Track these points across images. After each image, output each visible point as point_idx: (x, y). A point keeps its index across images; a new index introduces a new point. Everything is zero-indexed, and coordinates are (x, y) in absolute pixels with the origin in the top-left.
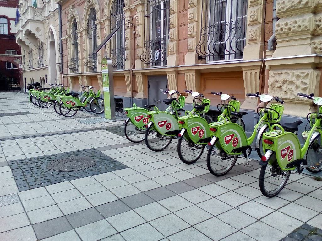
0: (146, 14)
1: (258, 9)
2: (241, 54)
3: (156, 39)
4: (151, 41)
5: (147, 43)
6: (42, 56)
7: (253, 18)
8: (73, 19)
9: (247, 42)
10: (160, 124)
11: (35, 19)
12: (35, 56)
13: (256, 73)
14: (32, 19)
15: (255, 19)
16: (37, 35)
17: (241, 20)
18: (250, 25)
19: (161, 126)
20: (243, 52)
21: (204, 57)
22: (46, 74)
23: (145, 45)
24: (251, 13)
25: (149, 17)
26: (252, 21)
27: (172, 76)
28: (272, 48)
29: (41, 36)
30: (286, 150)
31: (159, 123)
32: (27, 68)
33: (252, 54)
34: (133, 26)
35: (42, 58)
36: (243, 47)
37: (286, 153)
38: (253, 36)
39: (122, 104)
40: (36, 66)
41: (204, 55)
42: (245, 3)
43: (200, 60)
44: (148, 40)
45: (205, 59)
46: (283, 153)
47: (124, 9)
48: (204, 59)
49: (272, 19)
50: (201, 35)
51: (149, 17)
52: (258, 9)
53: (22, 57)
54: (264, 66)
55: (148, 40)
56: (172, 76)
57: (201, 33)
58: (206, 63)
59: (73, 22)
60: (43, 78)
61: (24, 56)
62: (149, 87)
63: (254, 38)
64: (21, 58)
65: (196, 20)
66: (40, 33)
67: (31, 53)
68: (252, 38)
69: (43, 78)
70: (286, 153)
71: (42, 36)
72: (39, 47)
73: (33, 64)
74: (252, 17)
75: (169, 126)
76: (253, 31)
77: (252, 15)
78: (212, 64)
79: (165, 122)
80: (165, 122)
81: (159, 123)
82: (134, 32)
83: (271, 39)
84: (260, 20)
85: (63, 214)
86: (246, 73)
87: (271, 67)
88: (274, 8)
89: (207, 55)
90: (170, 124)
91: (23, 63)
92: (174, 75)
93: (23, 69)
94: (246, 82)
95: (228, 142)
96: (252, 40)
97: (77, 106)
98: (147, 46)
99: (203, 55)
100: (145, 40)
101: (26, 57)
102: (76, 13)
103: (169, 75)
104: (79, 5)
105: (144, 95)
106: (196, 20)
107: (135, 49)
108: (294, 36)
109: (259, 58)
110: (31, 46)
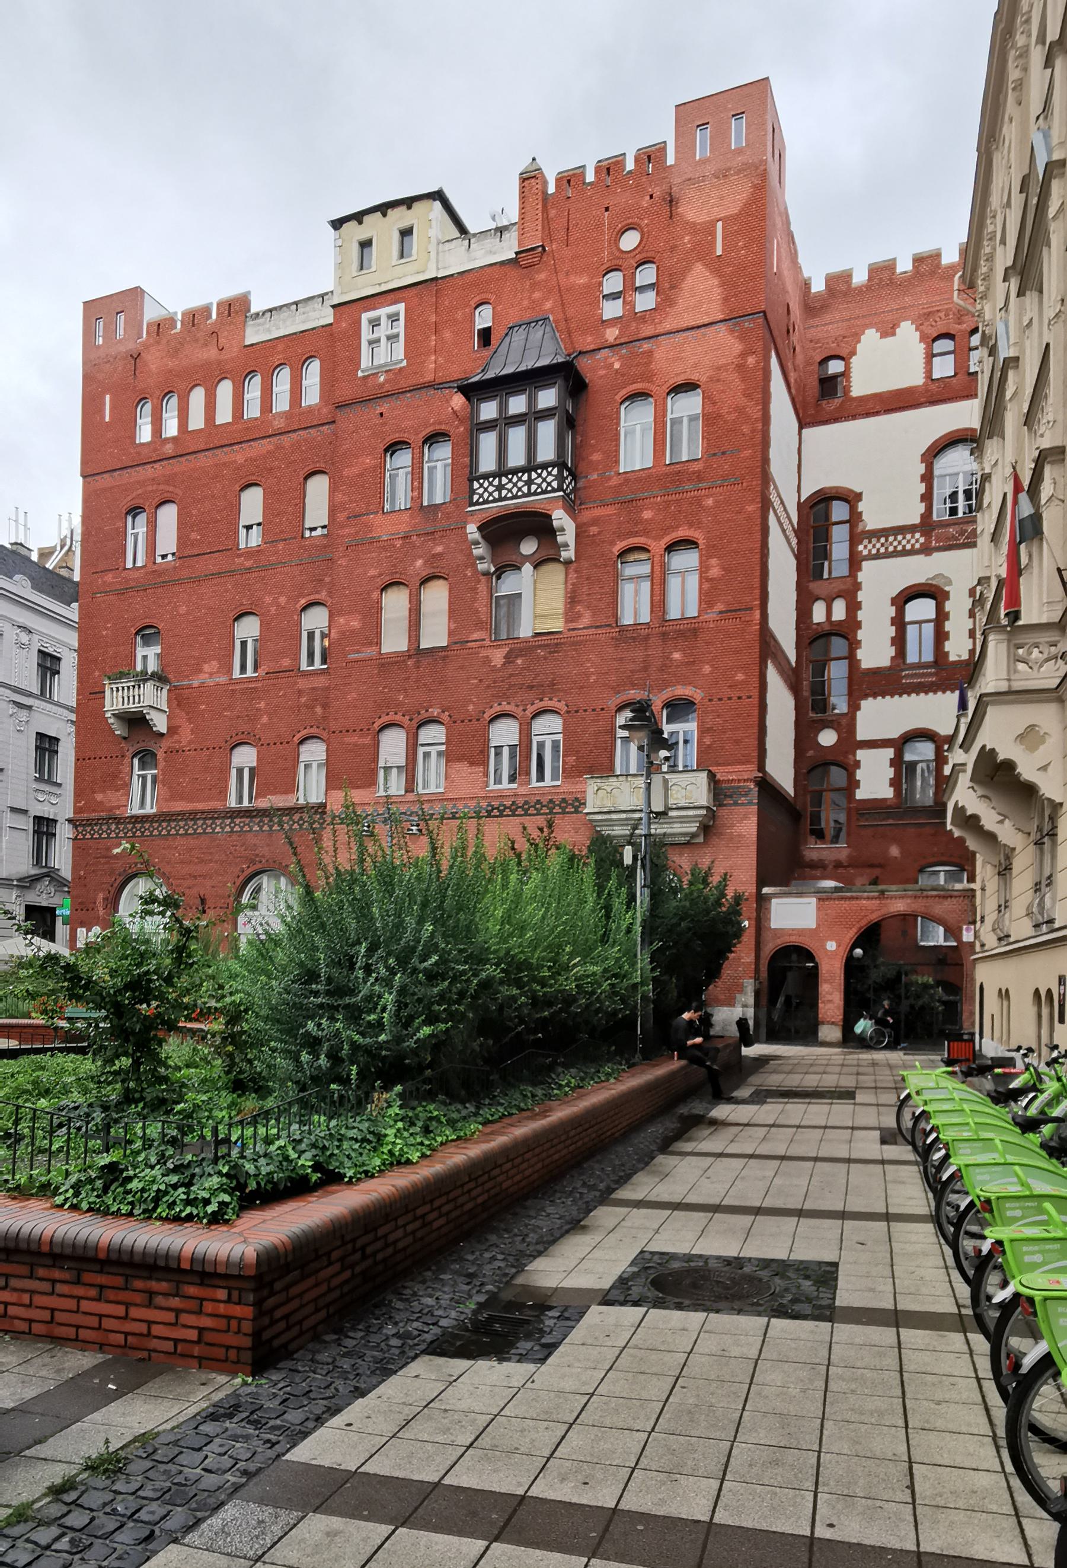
1: (1002, 1141)
6: (1050, 877)
11: (1017, 686)
12: (1022, 882)
14: (1003, 687)
16: (1027, 771)
22: (1062, 973)
29: (1044, 768)
32: (990, 940)
35: (1000, 906)
40: (1021, 929)
42: (657, 598)
48: (150, 1303)
52: (1002, 1141)
53: (978, 893)
60: (1049, 992)
61: (983, 889)
64: (974, 896)
66: (1042, 754)
67: (1004, 871)
69: (1049, 992)
71: (1050, 769)
72: (1040, 829)
73: (1054, 900)
85: (918, 1545)
91: (978, 918)
93: (978, 948)
101: (988, 892)
105: (1045, 1383)
110: (1007, 833)
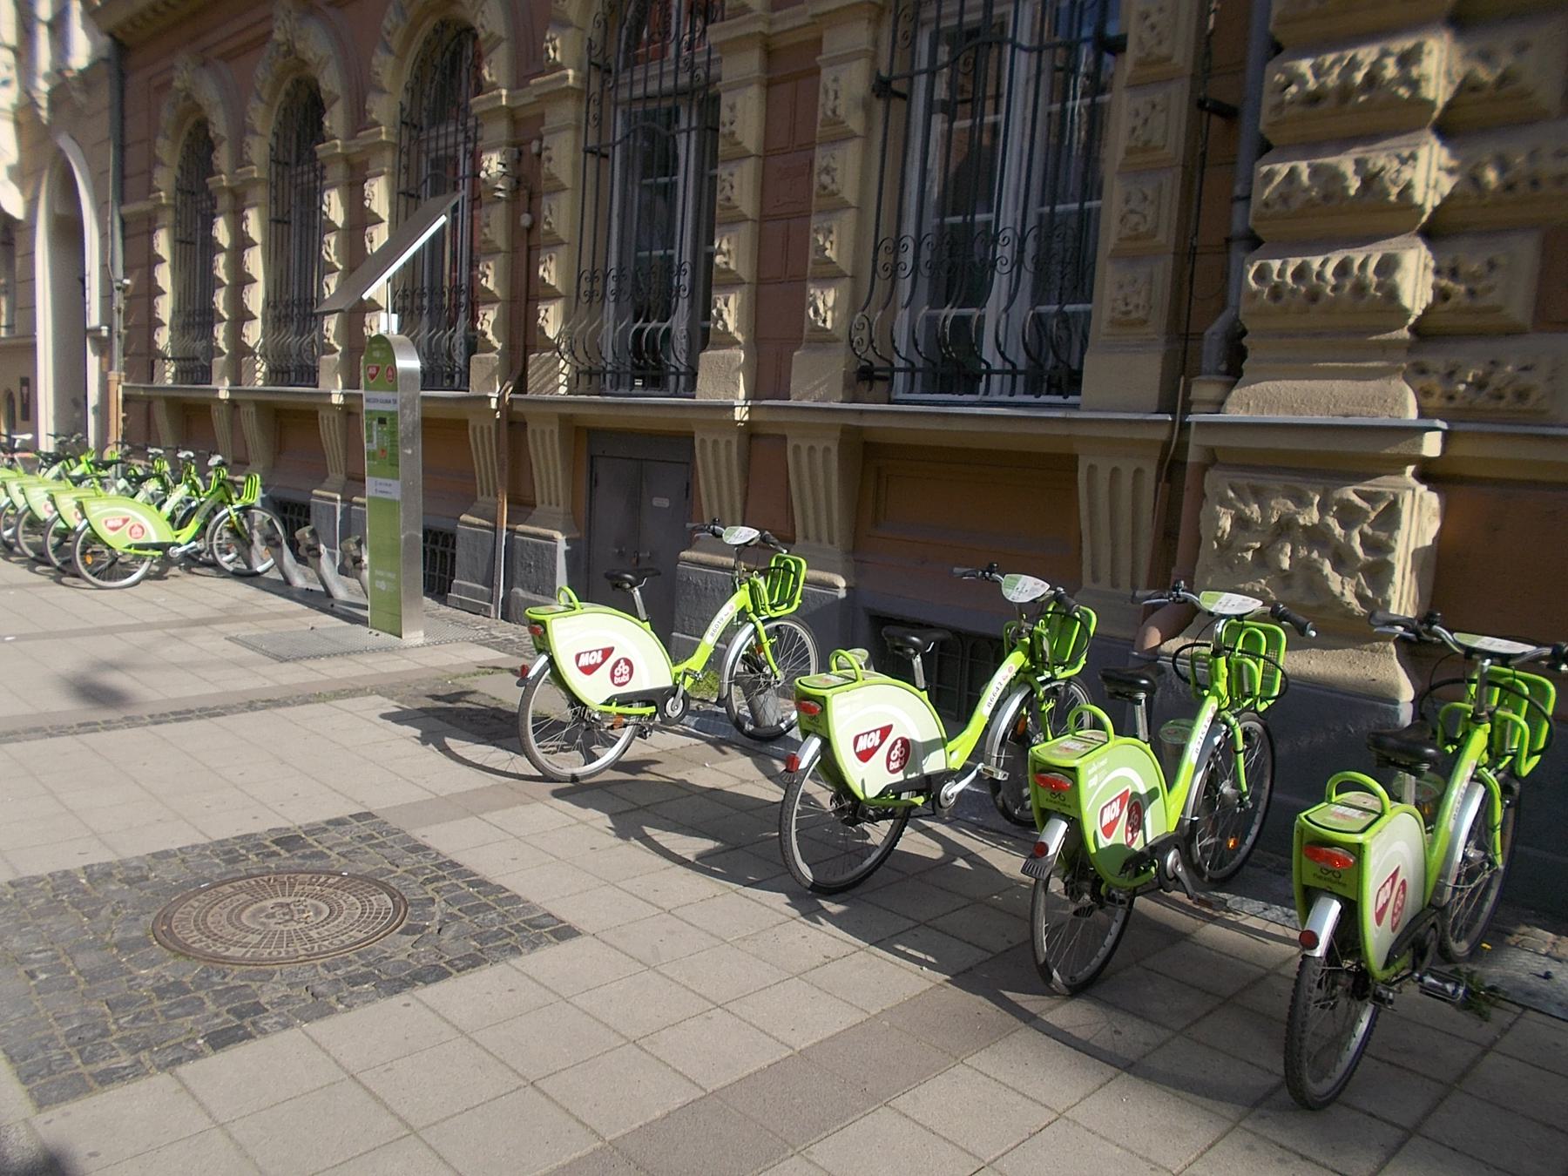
0: (592, 142)
2: (1070, 382)
3: (1032, 221)
4: (613, 273)
5: (593, 279)
7: (1138, 224)
8: (191, 120)
9: (1100, 329)
10: (584, 661)
13: (1138, 471)
15: (1142, 229)
17: (1073, 222)
18: (1116, 256)
19: (589, 670)
20: (1080, 372)
21: (887, 374)
22: (25, 375)
23: (585, 286)
24: (1127, 201)
25: (606, 156)
26: (1129, 238)
27: (722, 446)
28: (1223, 367)
30: (1116, 806)
31: (578, 657)
33: (1121, 381)
34: (524, 192)
36: (1082, 353)
37: (1116, 820)
38: (1130, 307)
39: (443, 554)
41: (886, 365)
43: (867, 383)
44: (599, 264)
45: (889, 380)
46: (1106, 820)
47: (479, 103)
49: (1228, 240)
50: (874, 271)
51: (606, 156)
54: (1183, 447)
55: (599, 264)
56: (722, 446)
57: (875, 261)
58: (890, 402)
59: (190, 134)
62: (593, 482)
63: (1134, 315)
65: (853, 202)
68: (1127, 313)
70: (1116, 820)
74: (1134, 218)
75: (623, 668)
76: (1124, 289)
77: (1132, 212)
78: (912, 412)
79: (607, 653)
80: (607, 653)
81: (578, 657)
82: (525, 220)
83: (1218, 326)
84: (1166, 237)
86: (1092, 468)
87: (1212, 459)
88: (1238, 190)
89: (900, 364)
90: (628, 662)
92: (728, 443)
94: (1092, 504)
95: (865, 756)
96: (1123, 323)
97: (155, 540)
98: (591, 294)
99: (878, 363)
100: (586, 265)
102: (209, 93)
103: (703, 441)
104: (227, 57)
106: (853, 202)
107: (527, 300)
108: (1316, 334)
109: (1154, 404)
